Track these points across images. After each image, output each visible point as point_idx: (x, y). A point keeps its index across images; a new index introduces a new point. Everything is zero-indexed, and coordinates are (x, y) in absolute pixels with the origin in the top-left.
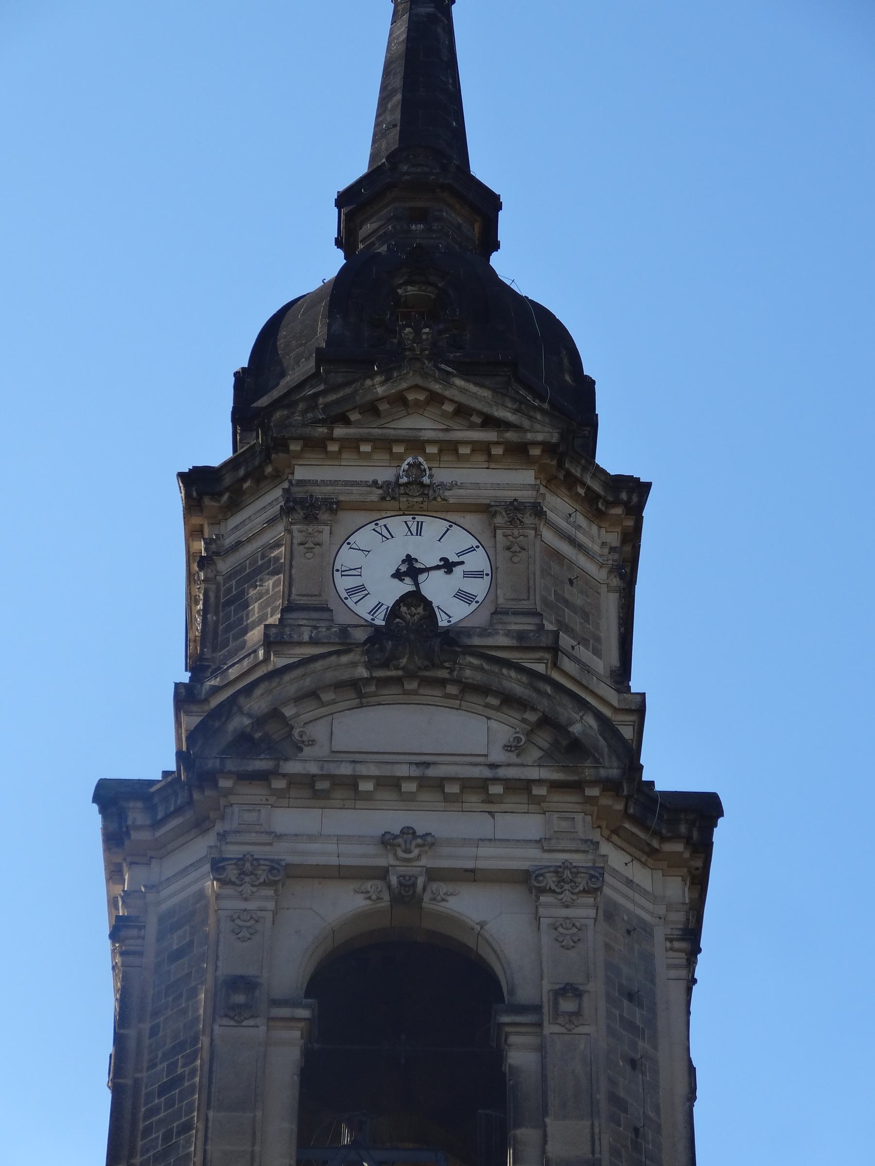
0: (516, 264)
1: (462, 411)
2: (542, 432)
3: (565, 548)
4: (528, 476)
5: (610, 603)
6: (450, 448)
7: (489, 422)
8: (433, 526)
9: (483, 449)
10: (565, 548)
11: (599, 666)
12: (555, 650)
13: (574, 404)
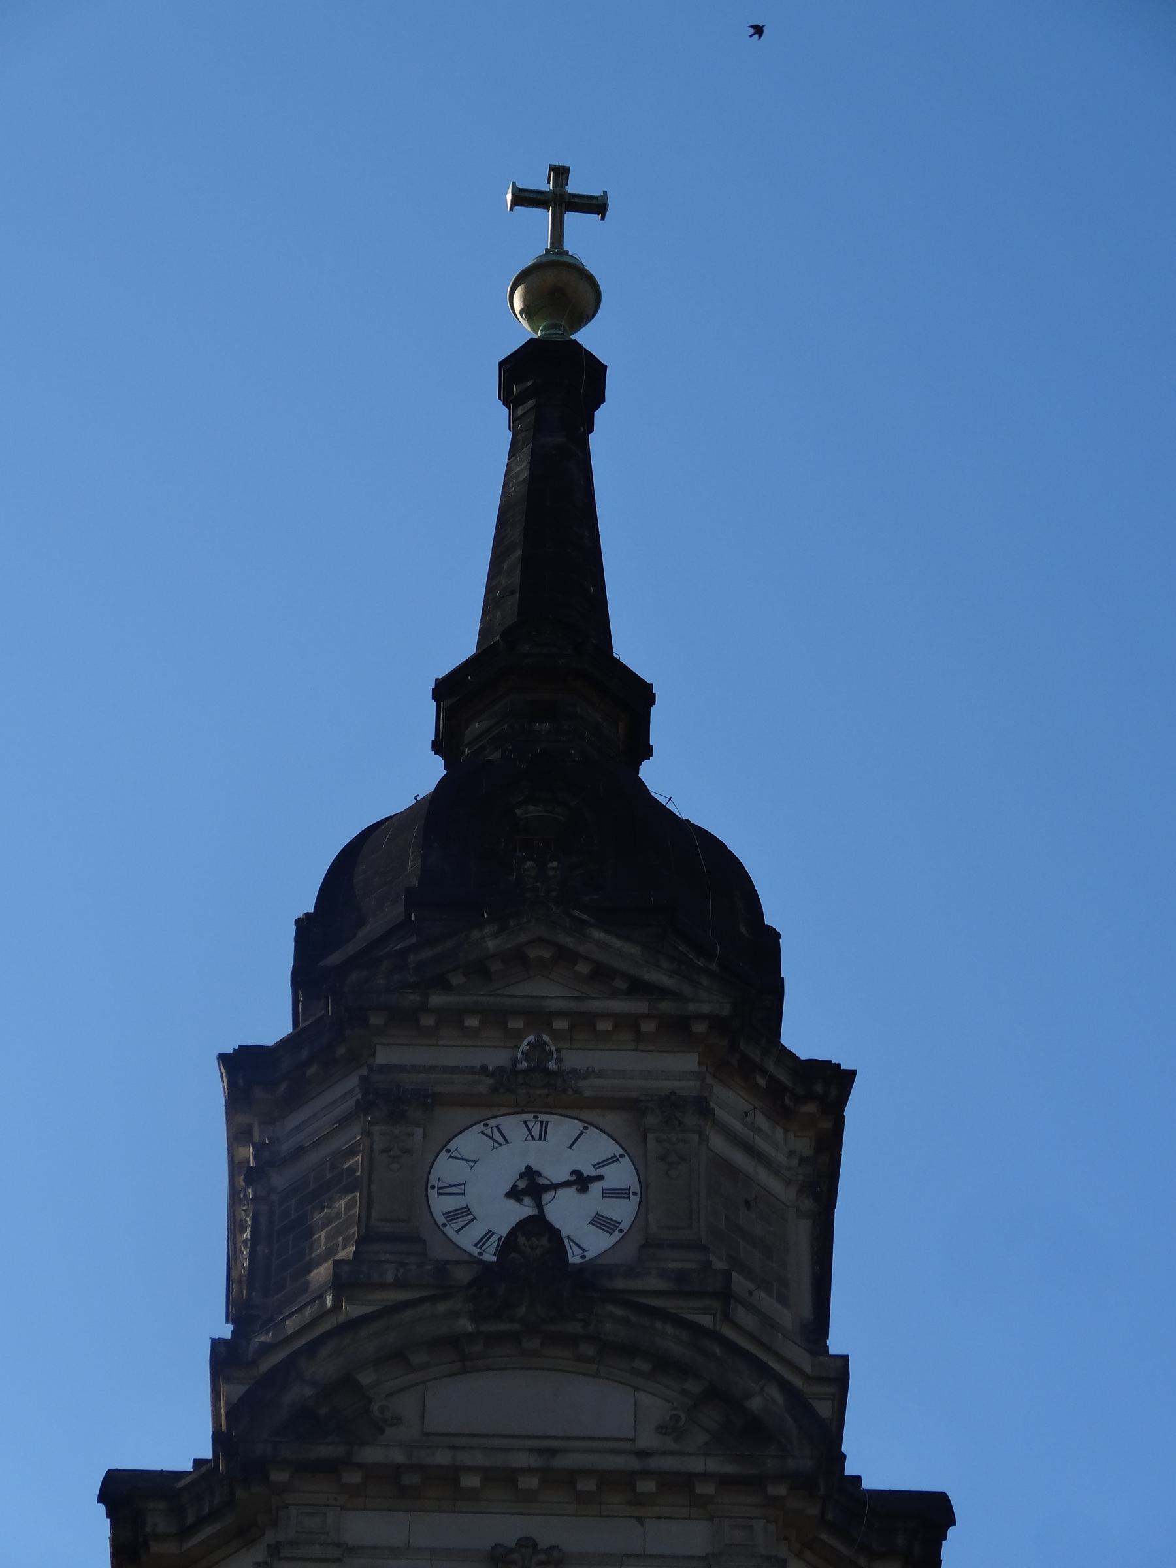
0: (680, 775)
1: (601, 974)
2: (709, 1002)
3: (739, 1158)
4: (689, 1061)
5: (801, 1233)
6: (584, 1023)
7: (637, 988)
8: (562, 1128)
9: (629, 1024)
10: (739, 1158)
11: (786, 1318)
12: (726, 1296)
13: (750, 961)
